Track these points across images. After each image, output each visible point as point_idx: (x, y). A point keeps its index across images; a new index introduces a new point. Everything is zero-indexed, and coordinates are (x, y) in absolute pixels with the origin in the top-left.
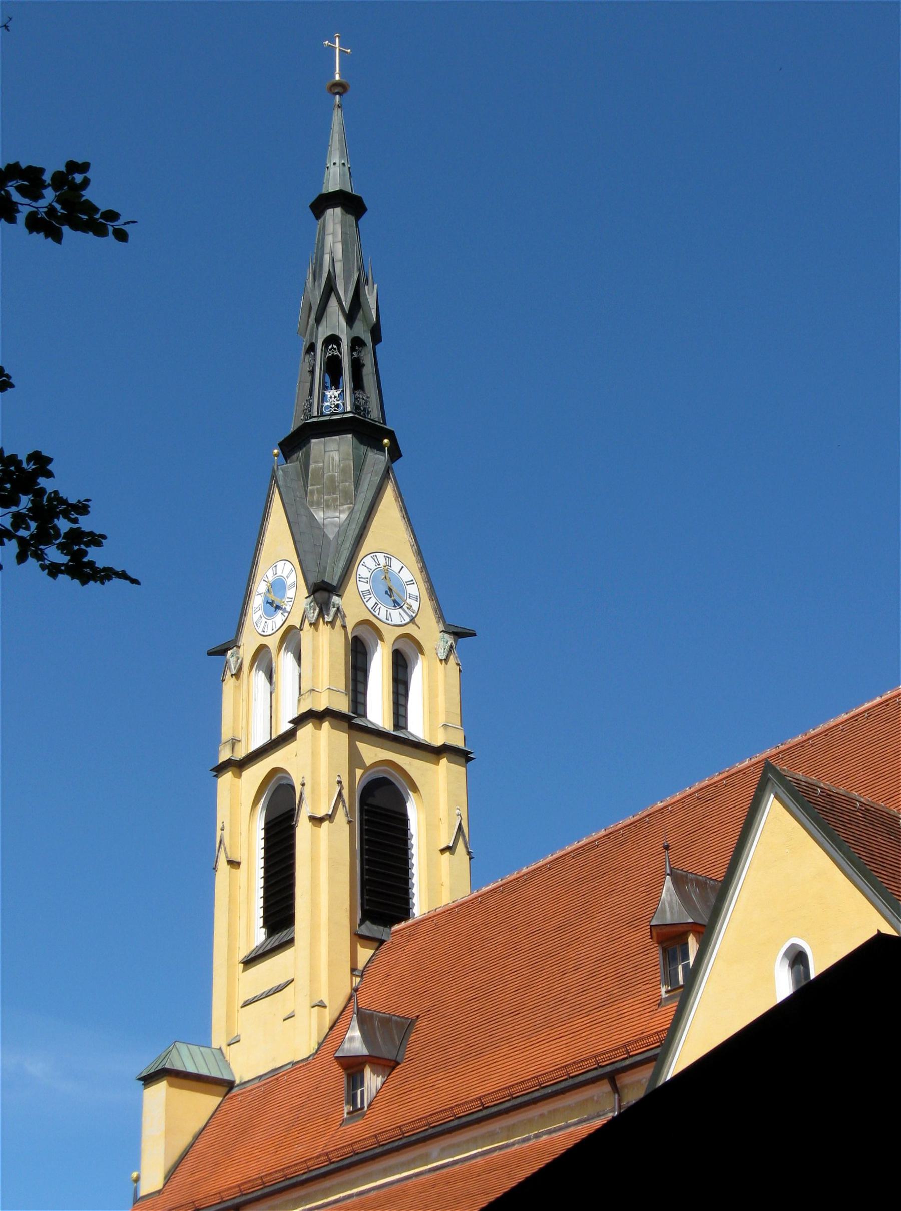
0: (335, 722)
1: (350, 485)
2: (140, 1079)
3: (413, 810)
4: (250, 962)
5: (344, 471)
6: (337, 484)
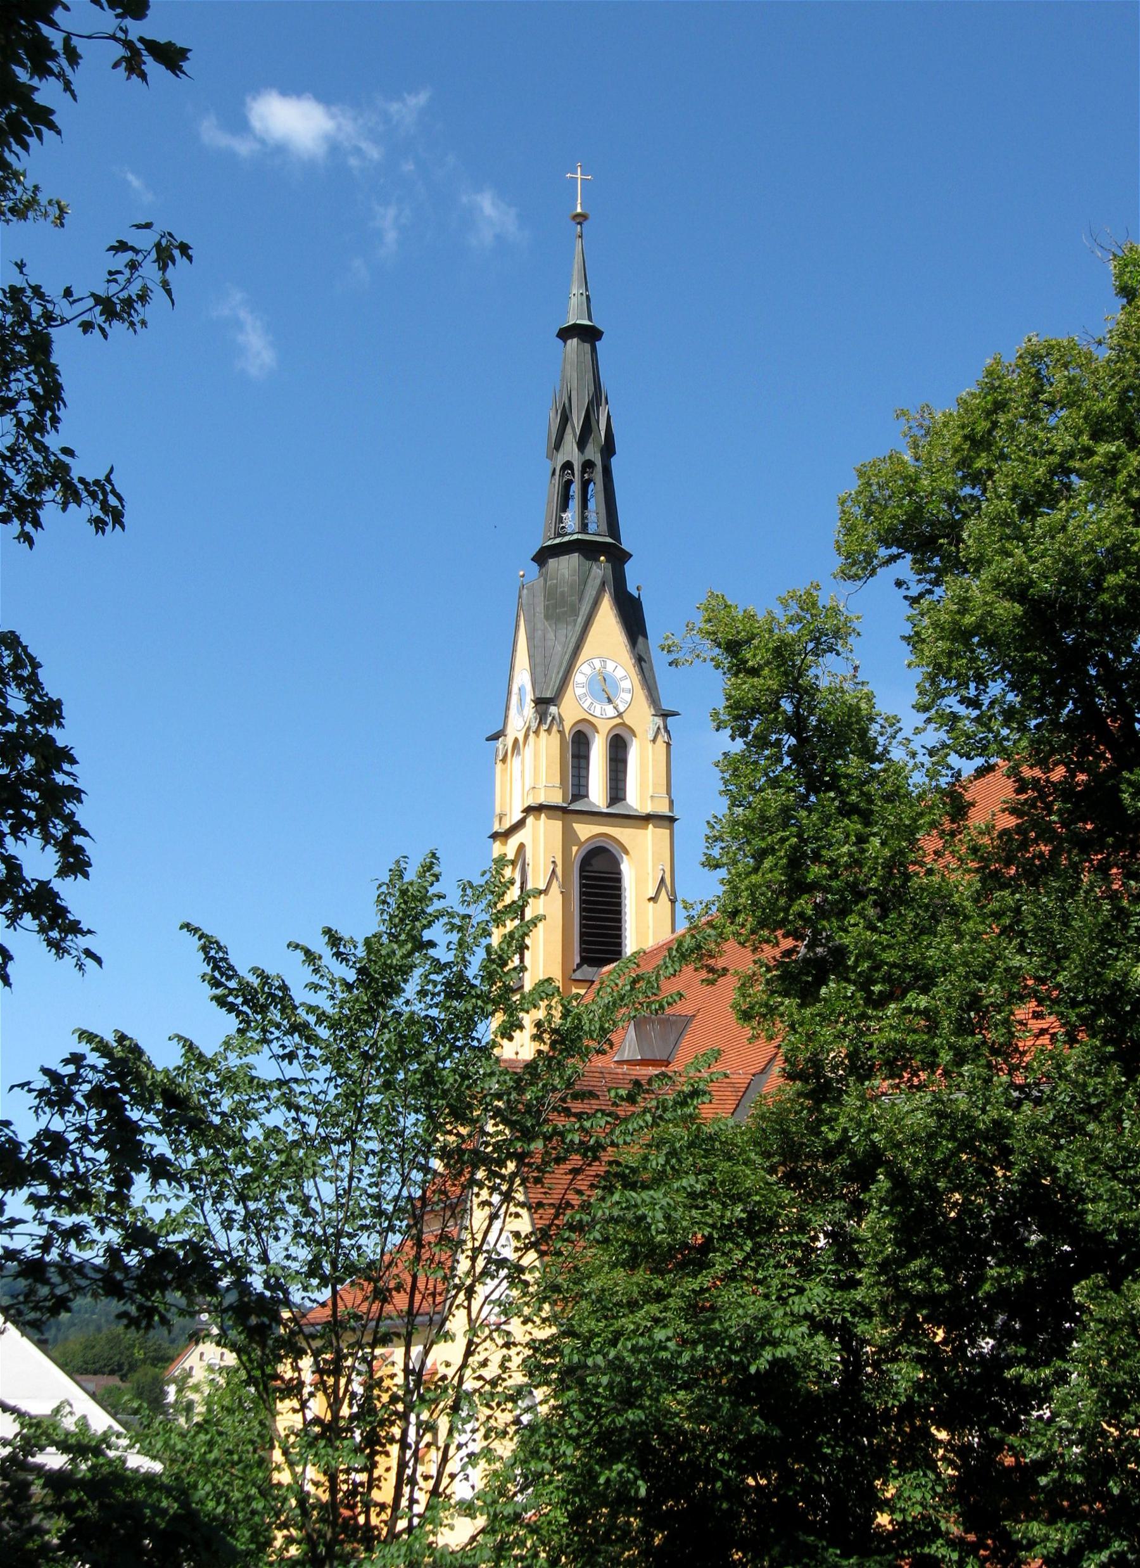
0: (551, 813)
1: (575, 598)
3: (627, 868)
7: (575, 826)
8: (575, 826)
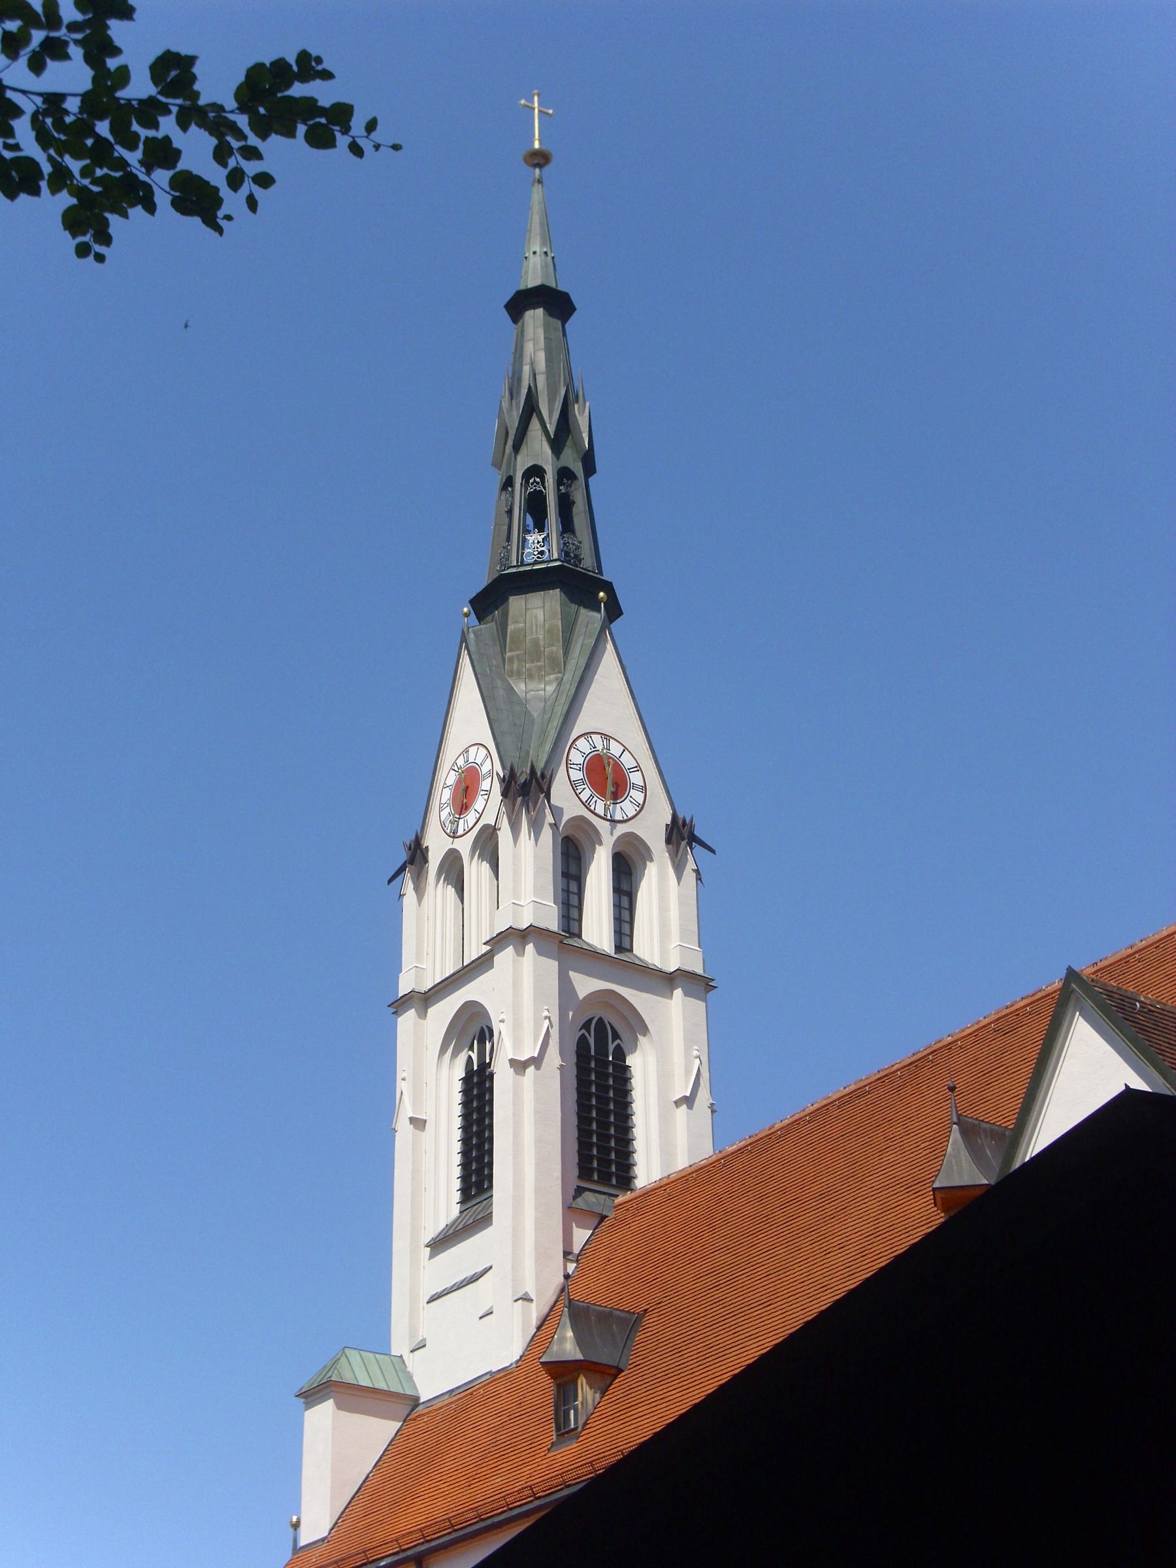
1: (558, 649)
4: (440, 1244)
5: (550, 632)
6: (542, 649)
7: (571, 973)
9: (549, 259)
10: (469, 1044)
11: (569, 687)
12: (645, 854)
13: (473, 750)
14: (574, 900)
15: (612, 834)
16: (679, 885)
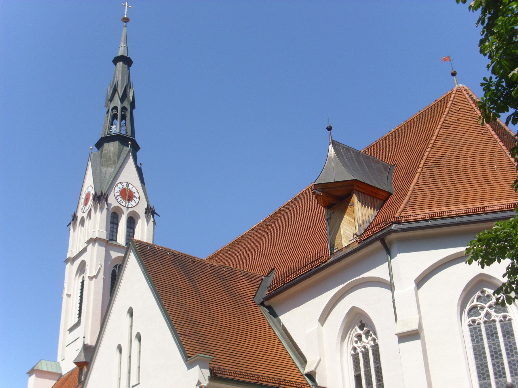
1: (116, 158)
2: (27, 373)
4: (71, 330)
5: (114, 154)
6: (112, 158)
7: (111, 252)
8: (111, 252)
9: (126, 48)
10: (83, 272)
11: (117, 169)
12: (138, 217)
13: (89, 187)
14: (115, 230)
15: (127, 211)
16: (147, 225)
